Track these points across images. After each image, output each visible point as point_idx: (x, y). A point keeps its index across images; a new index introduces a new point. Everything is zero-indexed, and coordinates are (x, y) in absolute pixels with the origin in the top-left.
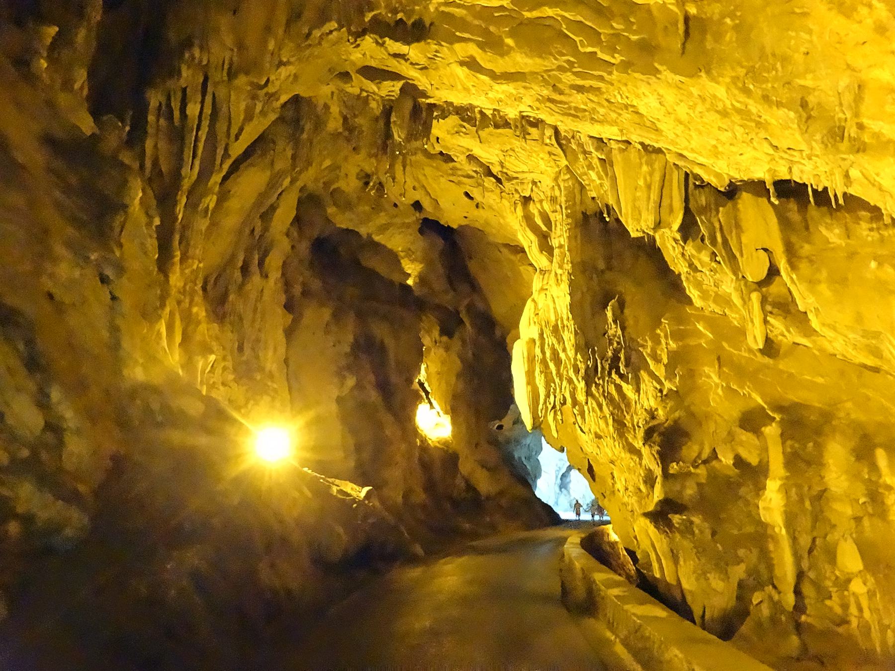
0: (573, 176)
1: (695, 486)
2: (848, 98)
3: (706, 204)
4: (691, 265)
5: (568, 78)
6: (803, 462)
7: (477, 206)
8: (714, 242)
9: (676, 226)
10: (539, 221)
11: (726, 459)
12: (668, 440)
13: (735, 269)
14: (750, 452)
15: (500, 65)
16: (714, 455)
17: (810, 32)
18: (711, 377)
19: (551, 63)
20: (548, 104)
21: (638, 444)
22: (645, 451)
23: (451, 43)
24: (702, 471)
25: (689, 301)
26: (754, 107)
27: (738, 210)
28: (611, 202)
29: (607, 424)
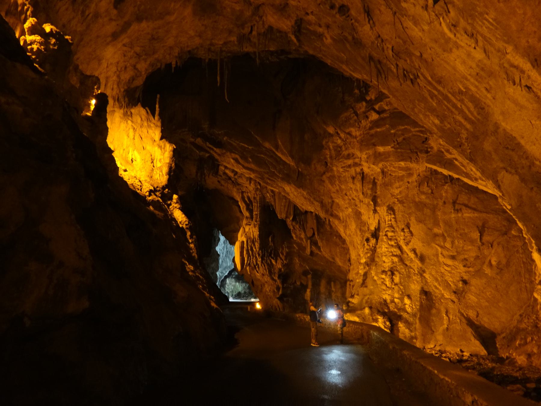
0: (262, 194)
2: (330, 205)
3: (299, 215)
4: (294, 227)
5: (267, 176)
6: (316, 285)
8: (300, 224)
9: (291, 219)
10: (246, 199)
11: (298, 283)
12: (284, 277)
13: (305, 232)
15: (246, 165)
16: (295, 282)
17: (324, 187)
18: (297, 260)
19: (262, 170)
21: (276, 278)
22: (278, 281)
24: (292, 286)
25: (292, 237)
26: (312, 200)
28: (273, 204)
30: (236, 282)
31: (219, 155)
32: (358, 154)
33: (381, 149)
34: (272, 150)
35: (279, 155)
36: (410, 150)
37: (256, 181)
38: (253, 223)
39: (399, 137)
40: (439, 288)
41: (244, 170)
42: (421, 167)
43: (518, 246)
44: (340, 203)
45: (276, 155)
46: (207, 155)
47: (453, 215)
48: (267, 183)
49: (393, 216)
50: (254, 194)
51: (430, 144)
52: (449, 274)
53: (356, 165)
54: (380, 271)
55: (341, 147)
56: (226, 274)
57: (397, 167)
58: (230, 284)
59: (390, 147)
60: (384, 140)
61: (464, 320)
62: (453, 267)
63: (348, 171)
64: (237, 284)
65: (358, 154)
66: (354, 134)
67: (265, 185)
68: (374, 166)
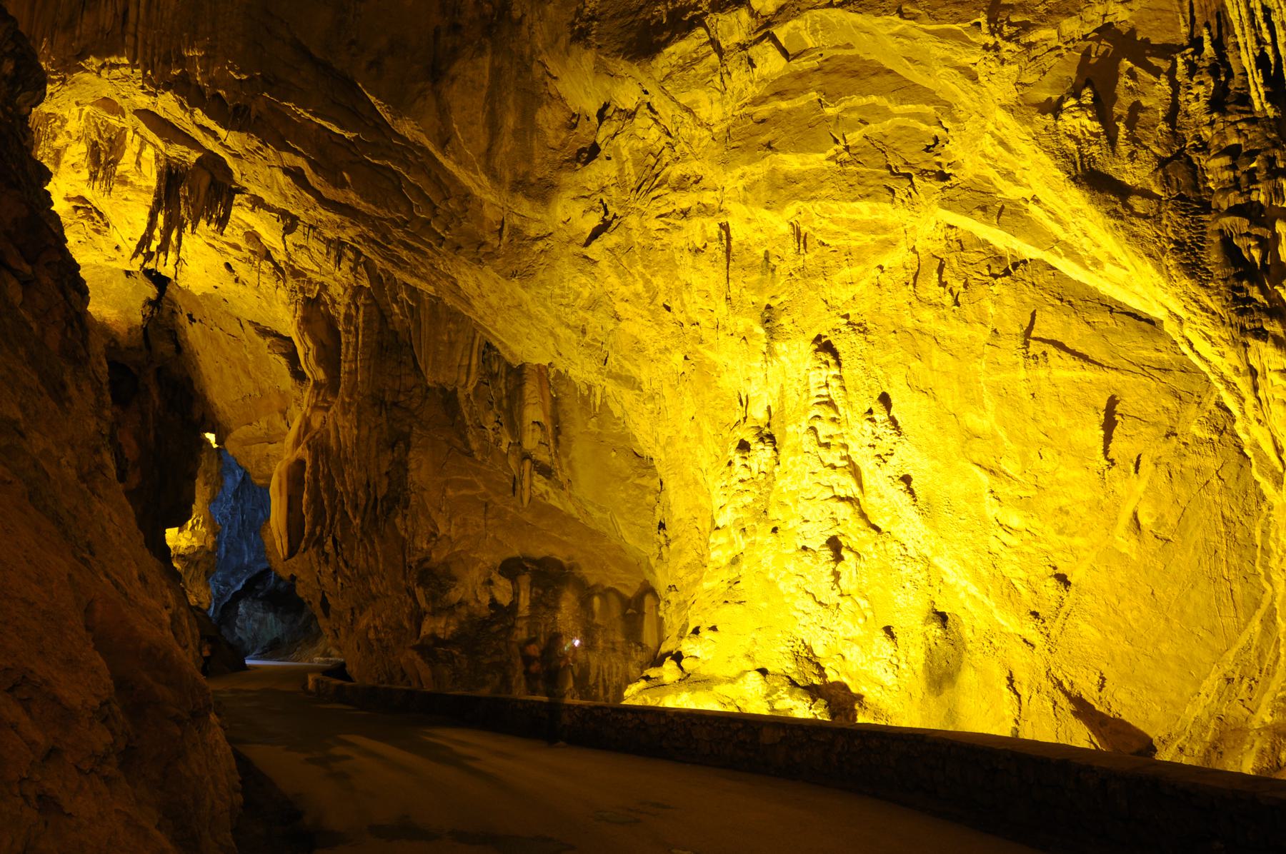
5: (398, 233)
7: (236, 280)
15: (330, 193)
19: (382, 213)
27: (521, 398)
29: (377, 560)
31: (237, 156)
32: (712, 174)
33: (792, 162)
34: (423, 149)
35: (449, 164)
36: (889, 167)
37: (358, 254)
38: (338, 401)
39: (852, 128)
40: (986, 601)
41: (323, 214)
42: (926, 222)
43: (1208, 469)
46: (194, 157)
47: (1022, 374)
49: (835, 371)
50: (348, 306)
51: (949, 154)
52: (1015, 558)
53: (704, 210)
54: (792, 550)
55: (658, 156)
56: (239, 587)
57: (841, 216)
59: (822, 156)
60: (806, 133)
61: (1064, 702)
62: (1027, 535)
63: (680, 228)
64: (271, 616)
65: (712, 174)
66: (703, 113)
67: (389, 266)
68: (768, 215)
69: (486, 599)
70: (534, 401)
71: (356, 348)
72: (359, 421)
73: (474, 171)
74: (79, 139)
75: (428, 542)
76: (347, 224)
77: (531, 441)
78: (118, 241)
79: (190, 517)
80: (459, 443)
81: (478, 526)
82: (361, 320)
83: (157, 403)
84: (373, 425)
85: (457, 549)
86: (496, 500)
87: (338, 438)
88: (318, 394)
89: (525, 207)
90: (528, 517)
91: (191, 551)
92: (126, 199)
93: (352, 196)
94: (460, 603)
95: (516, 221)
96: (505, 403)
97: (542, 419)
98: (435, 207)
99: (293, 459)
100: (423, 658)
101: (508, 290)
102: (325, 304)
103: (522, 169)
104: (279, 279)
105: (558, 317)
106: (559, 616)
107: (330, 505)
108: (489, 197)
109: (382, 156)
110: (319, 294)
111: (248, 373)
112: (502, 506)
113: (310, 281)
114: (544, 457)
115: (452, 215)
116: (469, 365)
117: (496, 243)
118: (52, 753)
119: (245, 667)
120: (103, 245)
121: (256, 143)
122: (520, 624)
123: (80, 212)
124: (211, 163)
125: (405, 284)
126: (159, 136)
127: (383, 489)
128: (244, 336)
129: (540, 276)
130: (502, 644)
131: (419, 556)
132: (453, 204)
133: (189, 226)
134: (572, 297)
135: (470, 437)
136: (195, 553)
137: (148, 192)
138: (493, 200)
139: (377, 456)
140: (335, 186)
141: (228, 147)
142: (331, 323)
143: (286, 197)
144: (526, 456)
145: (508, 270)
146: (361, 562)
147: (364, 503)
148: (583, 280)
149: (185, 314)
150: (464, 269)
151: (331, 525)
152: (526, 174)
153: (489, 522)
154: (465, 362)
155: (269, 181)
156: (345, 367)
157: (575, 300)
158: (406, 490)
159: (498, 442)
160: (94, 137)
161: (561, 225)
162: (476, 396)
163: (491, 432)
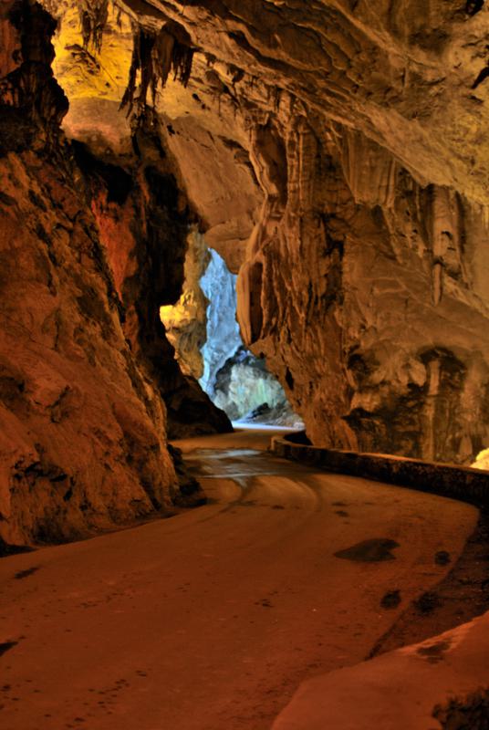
1: (379, 399)
5: (321, 83)
14: (419, 377)
19: (307, 67)
20: (302, 91)
23: (224, 18)
27: (432, 213)
29: (319, 346)
30: (256, 377)
31: (192, 24)
35: (358, 24)
38: (285, 217)
41: (262, 69)
44: (427, 407)
45: (351, 24)
46: (160, 24)
48: (324, 105)
50: (291, 134)
56: (232, 354)
58: (241, 381)
64: (261, 381)
67: (317, 107)
69: (405, 380)
70: (442, 214)
71: (298, 171)
72: (302, 233)
73: (379, 29)
74: (73, 6)
75: (359, 332)
76: (281, 76)
77: (440, 248)
78: (108, 80)
79: (182, 293)
80: (385, 249)
81: (399, 319)
82: (301, 146)
83: (148, 198)
84: (313, 236)
85: (381, 339)
86: (414, 297)
87: (286, 246)
88: (272, 207)
89: (422, 57)
90: (441, 311)
91: (184, 323)
92: (112, 46)
93: (283, 54)
94: (383, 383)
95: (415, 68)
96: (419, 216)
97: (450, 230)
98: (349, 60)
99: (253, 262)
100: (350, 426)
101: (411, 127)
102: (275, 128)
103: (419, 22)
104: (236, 108)
105: (451, 150)
106: (462, 395)
107: (282, 300)
108: (392, 49)
109: (305, 19)
110: (269, 121)
111: (219, 179)
112: (419, 302)
113: (261, 111)
114: (453, 261)
115: (363, 66)
116: (388, 186)
117: (401, 88)
118: (107, 453)
119: (232, 430)
120: (97, 83)
121: (205, 14)
122: (429, 401)
123: (77, 57)
124: (173, 29)
125: (332, 120)
126: (134, 10)
127: (322, 290)
128: (214, 147)
129: (435, 116)
130: (416, 417)
131: (351, 344)
132: (364, 57)
133: (160, 81)
134: (462, 133)
135: (393, 244)
136: (188, 326)
137: (128, 38)
138: (396, 52)
139: (317, 262)
140: (270, 47)
141: (185, 17)
142: (280, 144)
143: (232, 54)
144: (438, 261)
145: (410, 111)
146: (308, 348)
147: (307, 300)
148: (471, 118)
149: (165, 125)
150: (375, 111)
151: (284, 316)
152: (423, 27)
153: (409, 316)
154: (384, 184)
155: (218, 43)
156: (290, 186)
157: (464, 136)
158: (340, 289)
159: (415, 248)
160: (85, 8)
161: (453, 70)
162: (397, 209)
163: (409, 239)
